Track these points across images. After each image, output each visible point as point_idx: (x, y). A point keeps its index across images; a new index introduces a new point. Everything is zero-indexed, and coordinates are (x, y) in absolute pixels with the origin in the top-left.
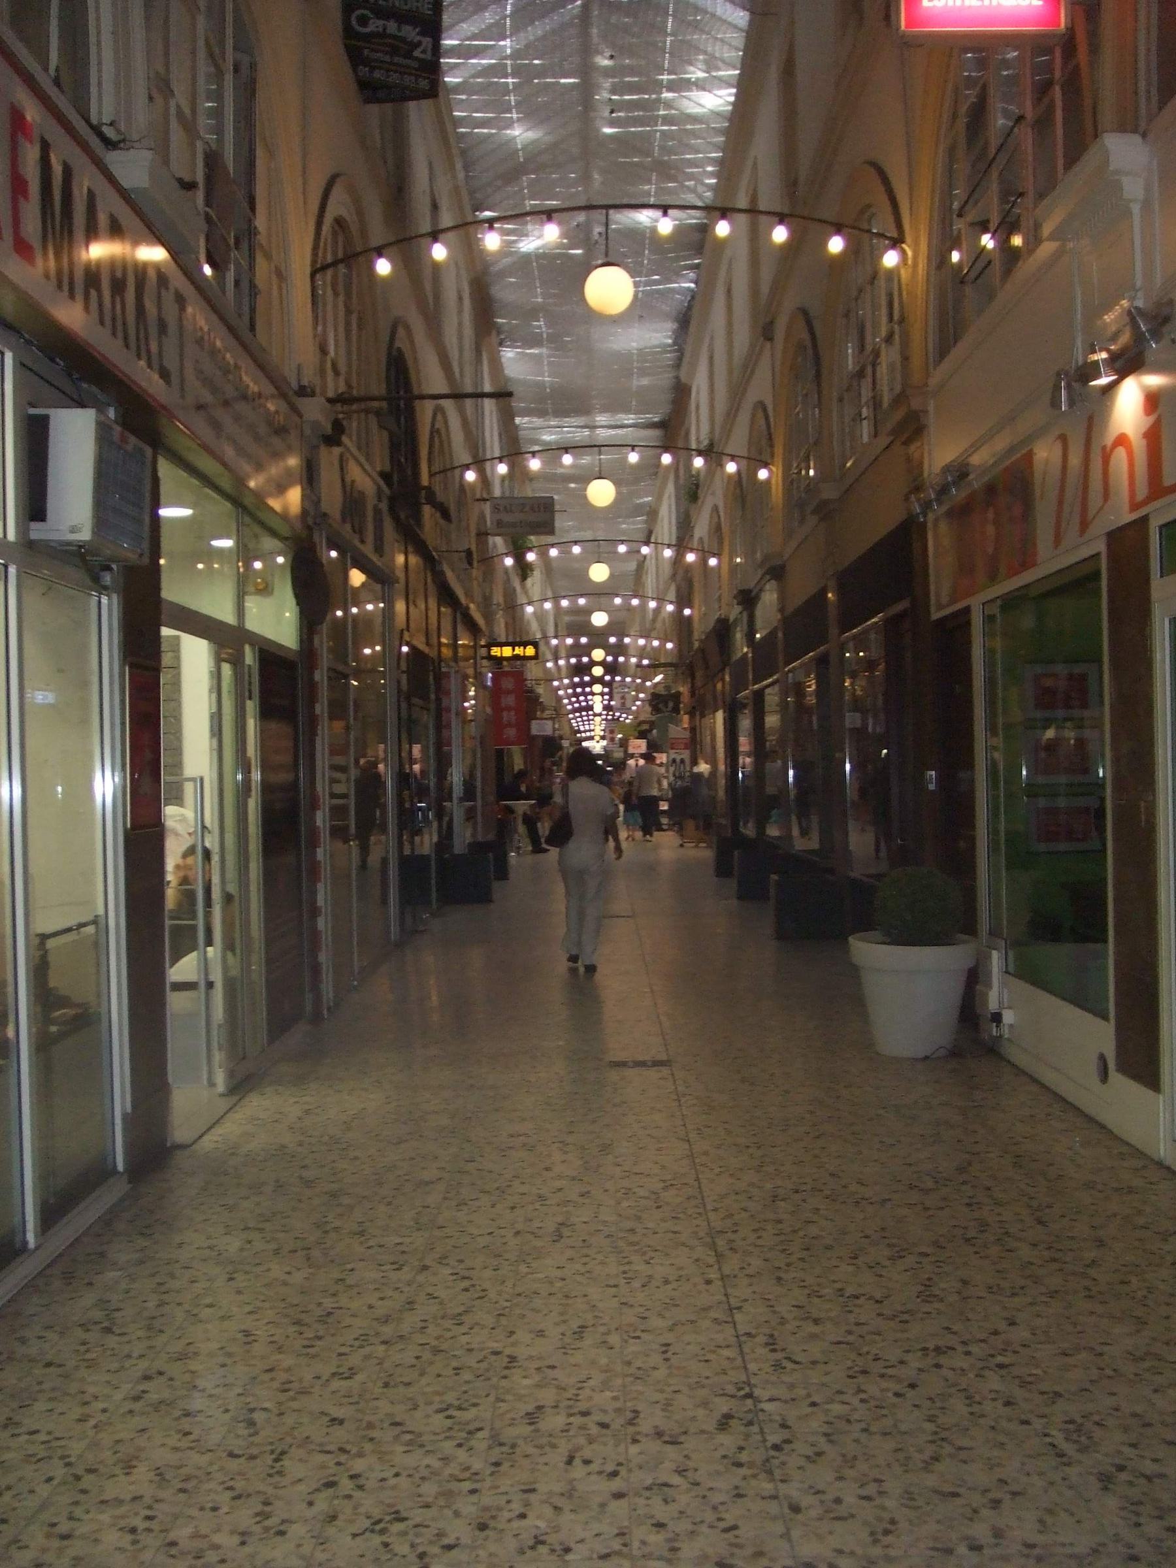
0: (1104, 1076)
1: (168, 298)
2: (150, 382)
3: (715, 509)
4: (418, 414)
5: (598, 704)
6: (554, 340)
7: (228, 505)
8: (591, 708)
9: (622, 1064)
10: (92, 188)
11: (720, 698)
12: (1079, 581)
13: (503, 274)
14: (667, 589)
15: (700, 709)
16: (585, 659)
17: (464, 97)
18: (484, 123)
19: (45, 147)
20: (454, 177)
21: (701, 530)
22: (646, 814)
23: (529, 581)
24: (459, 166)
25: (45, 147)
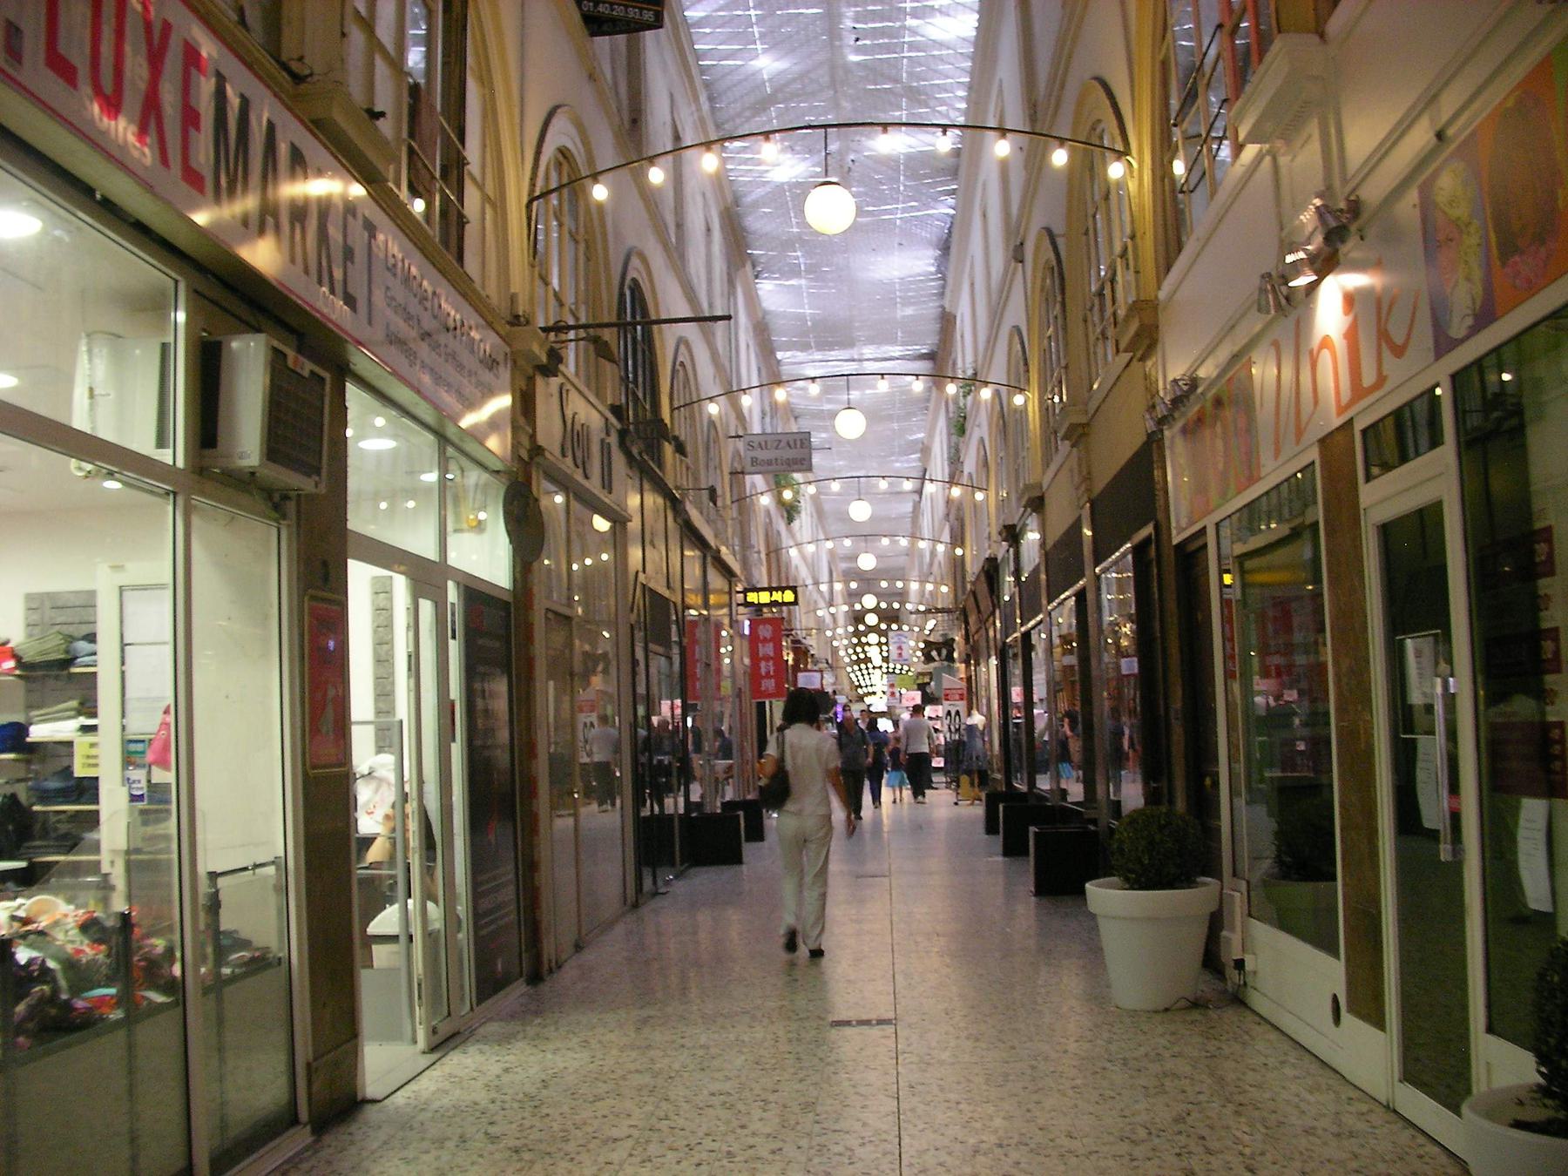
0: (1337, 1019)
1: (356, 226)
2: (334, 310)
3: (982, 440)
4: (657, 344)
5: (873, 652)
6: (811, 269)
7: (431, 437)
8: (868, 660)
9: (848, 1023)
10: (275, 120)
11: (992, 643)
12: (1295, 491)
13: (756, 205)
14: (942, 530)
15: (973, 656)
16: (858, 607)
17: (708, 30)
18: (731, 55)
19: (221, 80)
20: (699, 109)
21: (970, 465)
22: (918, 775)
23: (796, 524)
24: (703, 98)
25: (221, 80)
